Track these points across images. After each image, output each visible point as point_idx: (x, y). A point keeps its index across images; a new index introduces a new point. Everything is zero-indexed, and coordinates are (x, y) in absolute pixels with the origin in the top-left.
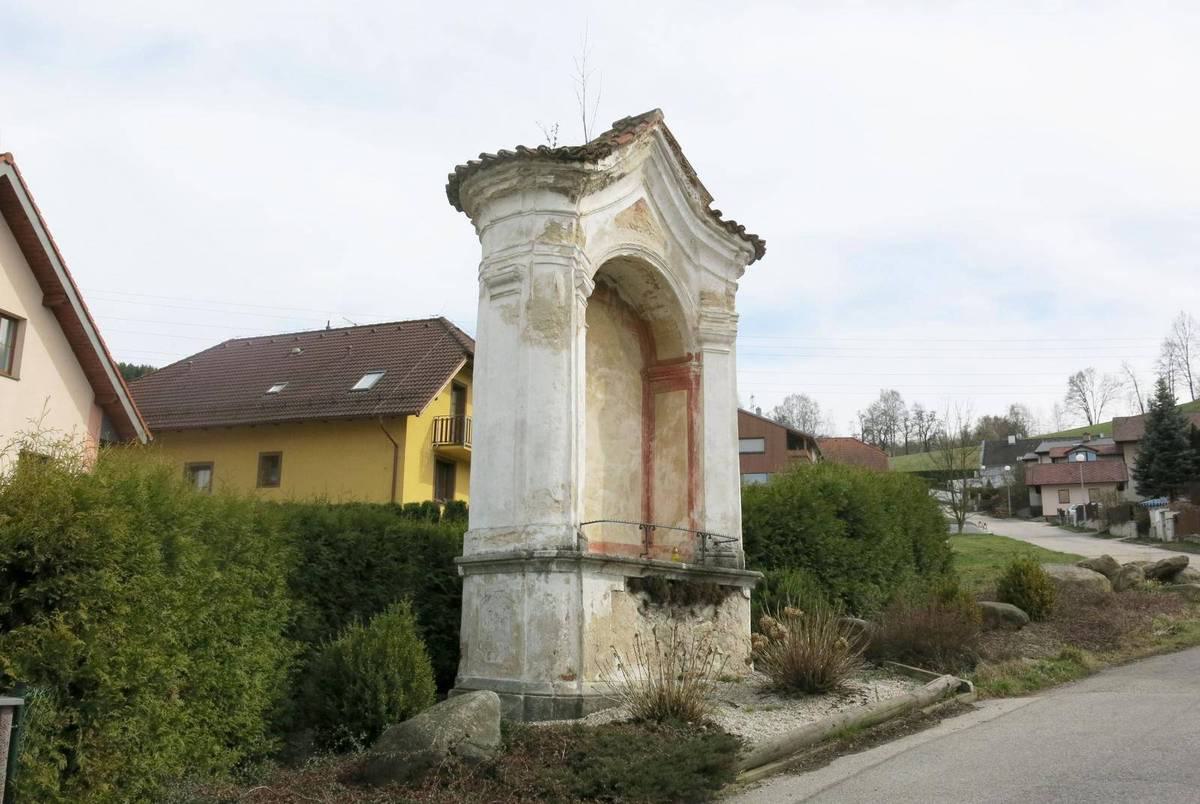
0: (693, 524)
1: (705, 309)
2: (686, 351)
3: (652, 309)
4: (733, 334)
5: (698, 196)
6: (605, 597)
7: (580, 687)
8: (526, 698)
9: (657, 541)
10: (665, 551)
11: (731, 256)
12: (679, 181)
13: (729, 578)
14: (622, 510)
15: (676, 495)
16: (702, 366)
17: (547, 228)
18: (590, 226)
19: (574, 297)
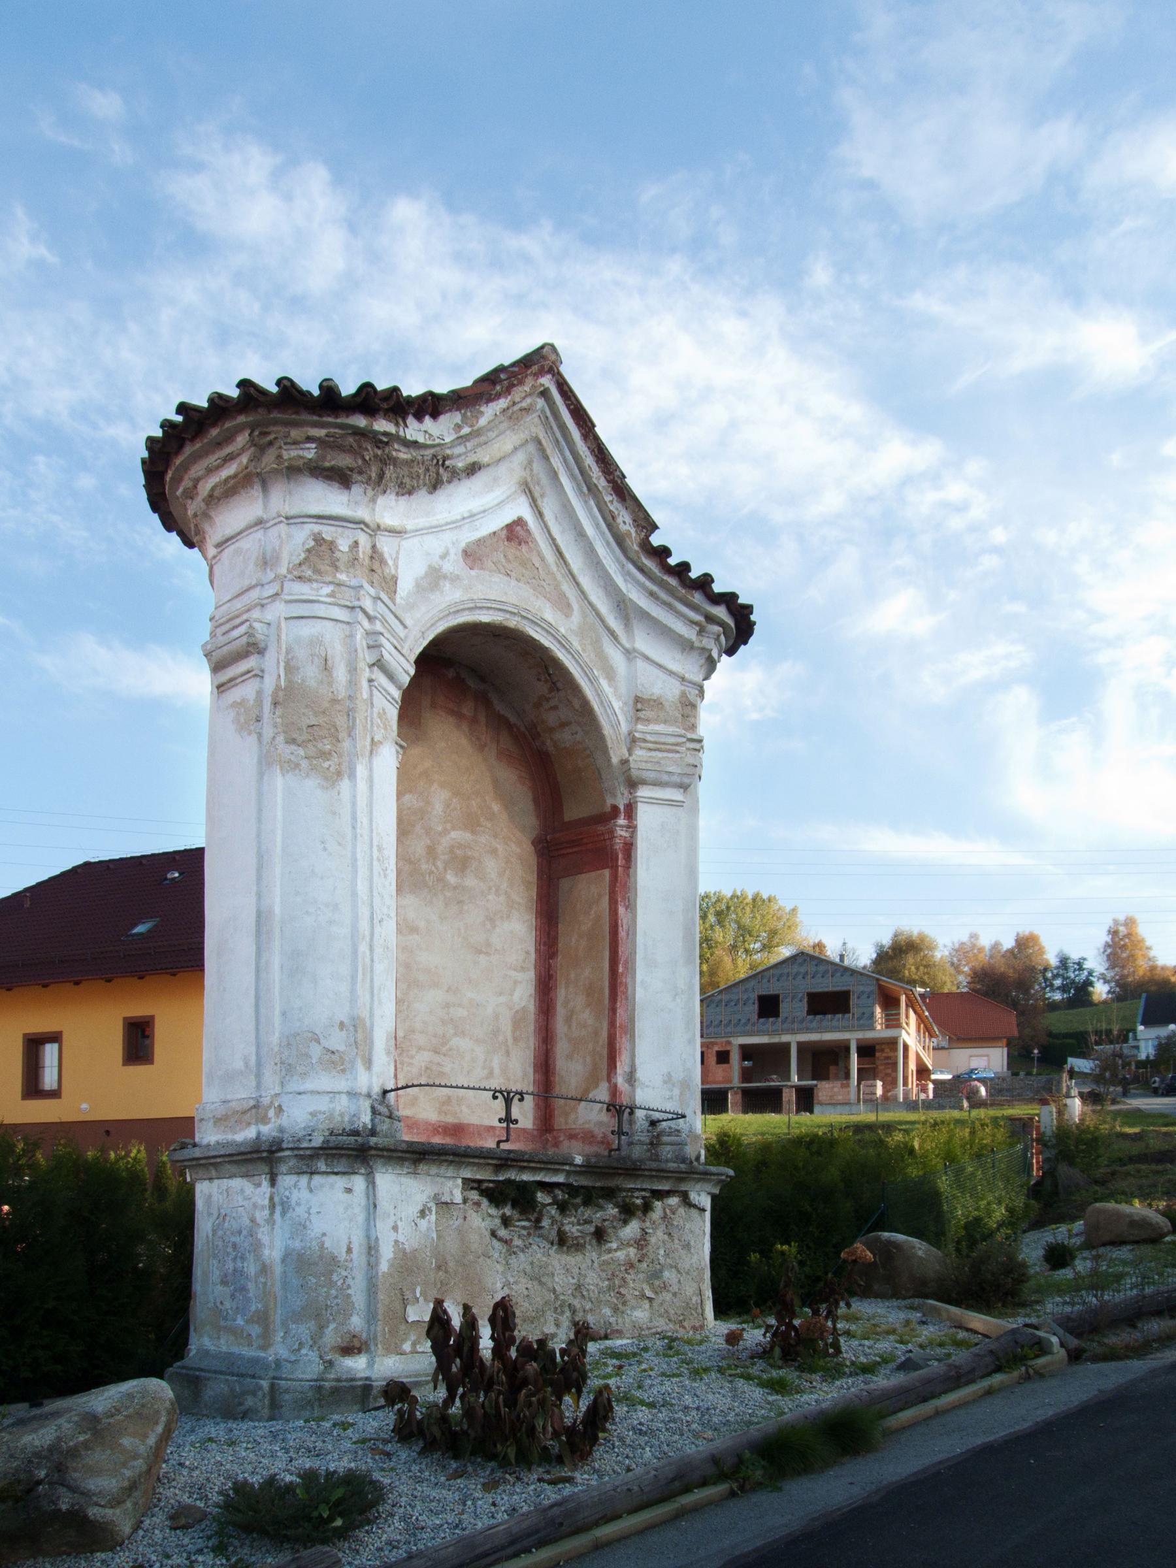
0: (614, 1091)
1: (640, 727)
2: (610, 801)
3: (551, 730)
4: (690, 770)
5: (628, 520)
6: (423, 1214)
7: (371, 1364)
8: (272, 1386)
9: (559, 1122)
10: (572, 1137)
11: (690, 633)
12: (592, 489)
13: (667, 1178)
14: (497, 1071)
15: (590, 1046)
16: (635, 827)
17: (309, 551)
18: (409, 563)
19: (365, 684)
